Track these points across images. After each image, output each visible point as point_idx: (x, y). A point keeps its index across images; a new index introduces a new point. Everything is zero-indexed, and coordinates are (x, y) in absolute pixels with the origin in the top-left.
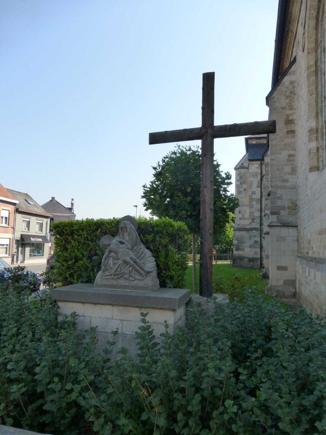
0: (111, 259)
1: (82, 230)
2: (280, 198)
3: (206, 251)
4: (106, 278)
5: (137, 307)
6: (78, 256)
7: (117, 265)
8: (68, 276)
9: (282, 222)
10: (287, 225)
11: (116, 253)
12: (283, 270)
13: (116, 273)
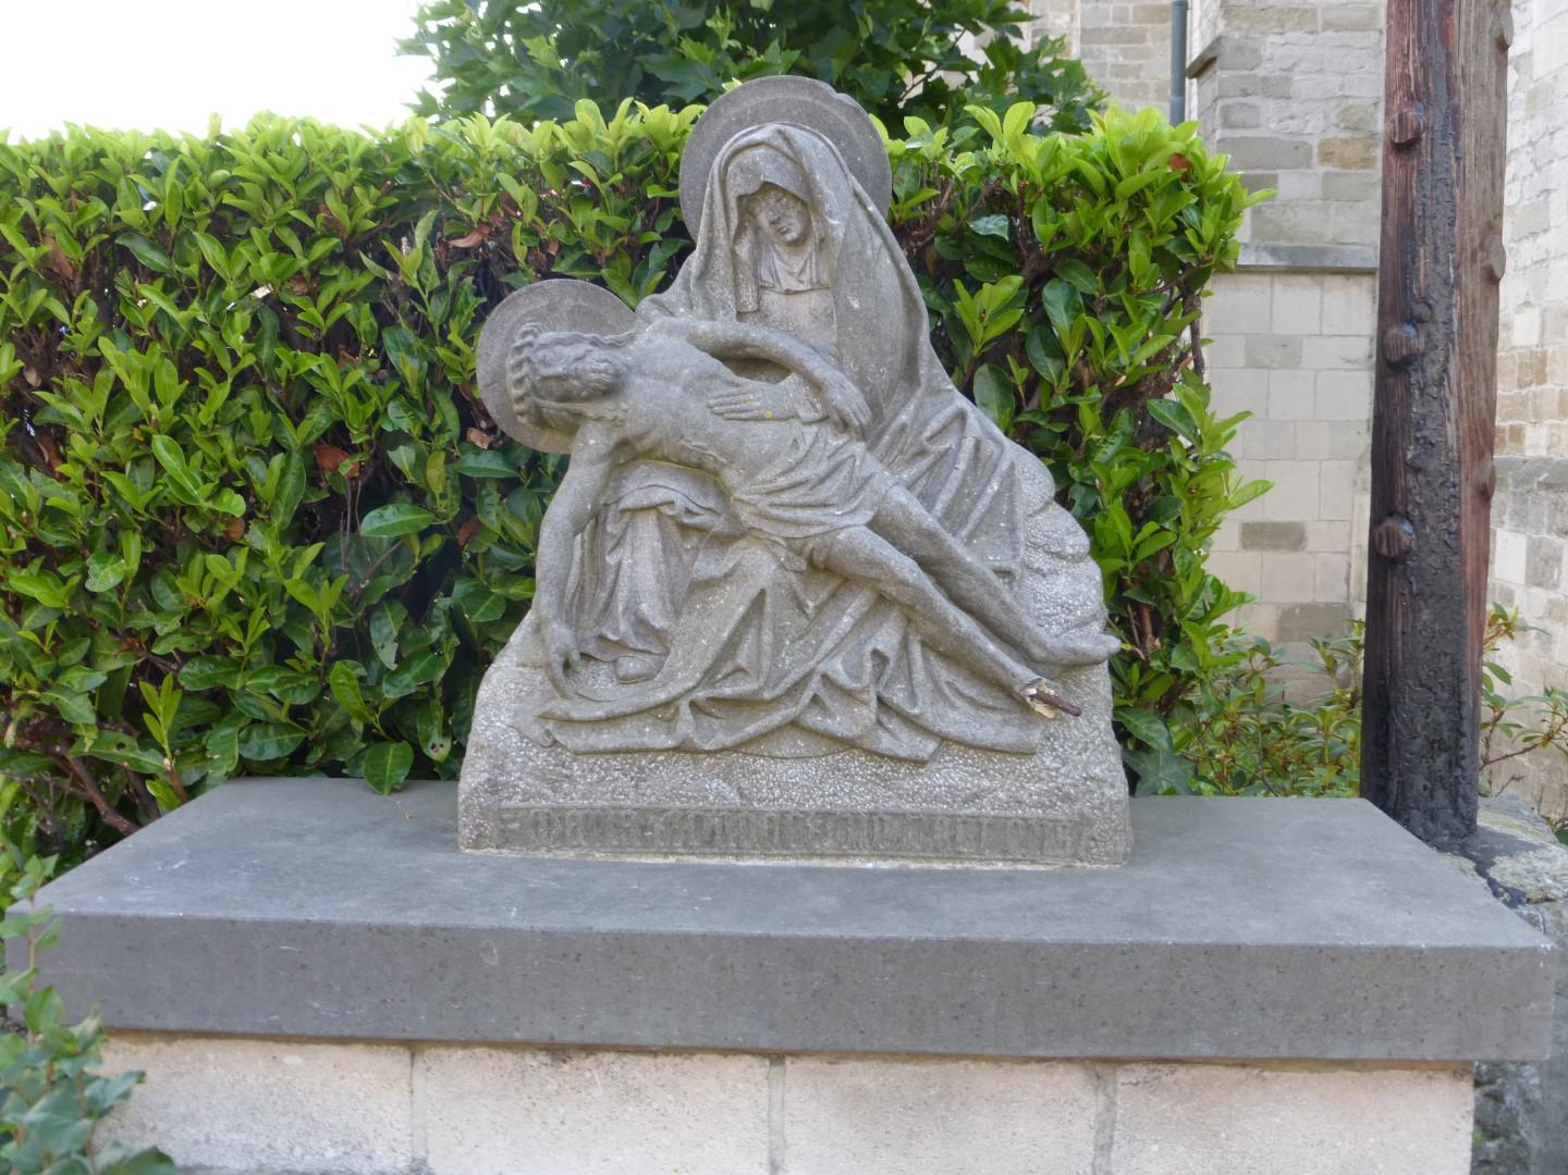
0: (647, 533)
1: (225, 227)
2: (1278, 88)
3: (1452, 442)
4: (608, 739)
5: (1069, 1060)
6: (194, 511)
7: (732, 604)
8: (79, 710)
9: (1283, 243)
10: (1315, 264)
11: (701, 471)
12: (1276, 547)
13: (727, 691)
